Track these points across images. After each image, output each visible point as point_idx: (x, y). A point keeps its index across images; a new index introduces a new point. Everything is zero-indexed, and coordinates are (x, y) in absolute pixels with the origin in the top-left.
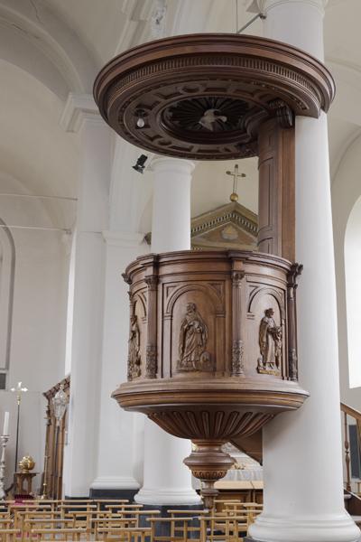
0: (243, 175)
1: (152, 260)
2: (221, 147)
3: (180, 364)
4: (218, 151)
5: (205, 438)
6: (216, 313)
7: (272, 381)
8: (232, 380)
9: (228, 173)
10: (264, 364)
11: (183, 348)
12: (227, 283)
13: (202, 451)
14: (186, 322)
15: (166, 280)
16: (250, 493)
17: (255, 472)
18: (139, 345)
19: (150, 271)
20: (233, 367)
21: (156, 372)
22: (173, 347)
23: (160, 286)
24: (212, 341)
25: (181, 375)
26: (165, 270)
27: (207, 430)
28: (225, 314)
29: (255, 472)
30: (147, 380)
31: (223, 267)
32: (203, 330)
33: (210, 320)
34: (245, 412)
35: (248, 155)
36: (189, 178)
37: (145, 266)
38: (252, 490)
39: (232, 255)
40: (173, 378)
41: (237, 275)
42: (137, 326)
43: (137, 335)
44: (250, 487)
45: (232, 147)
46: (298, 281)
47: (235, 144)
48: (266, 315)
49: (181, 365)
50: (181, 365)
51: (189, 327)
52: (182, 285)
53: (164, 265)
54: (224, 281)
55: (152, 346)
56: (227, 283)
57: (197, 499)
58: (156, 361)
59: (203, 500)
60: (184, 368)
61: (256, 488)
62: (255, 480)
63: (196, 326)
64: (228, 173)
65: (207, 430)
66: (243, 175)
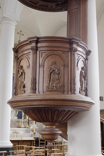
0: (23, 35)
1: (36, 39)
2: (50, 4)
3: (48, 87)
4: (47, 7)
5: (49, 122)
6: (64, 66)
7: (83, 98)
8: (73, 95)
9: (18, 33)
10: (82, 90)
11: (50, 80)
12: (69, 53)
13: (48, 128)
14: (51, 69)
15: (39, 49)
16: (20, 142)
17: (22, 134)
18: (24, 79)
19: (34, 45)
20: (73, 90)
21: (36, 91)
22: (44, 80)
23: (38, 52)
24: (62, 76)
25: (48, 93)
26: (39, 45)
27: (50, 119)
28: (68, 66)
29: (22, 134)
30: (31, 94)
31: (68, 46)
32: (59, 72)
33: (62, 68)
34: (68, 110)
35: (61, 10)
36: (15, 27)
37: (31, 42)
38: (21, 141)
39: (73, 40)
40: (42, 93)
41: (74, 50)
42: (23, 70)
43: (24, 74)
44: (21, 139)
45: (54, 5)
46: (89, 57)
47: (55, 4)
48: (82, 69)
49: (49, 88)
50: (49, 88)
51: (53, 71)
52: (49, 52)
53: (40, 43)
54: (68, 52)
55: (34, 79)
56: (69, 53)
57: (11, 145)
58: (36, 86)
59: (13, 146)
60: (50, 90)
61: (23, 140)
62: (22, 137)
63: (56, 71)
64: (18, 33)
65: (50, 119)
66: (23, 35)
